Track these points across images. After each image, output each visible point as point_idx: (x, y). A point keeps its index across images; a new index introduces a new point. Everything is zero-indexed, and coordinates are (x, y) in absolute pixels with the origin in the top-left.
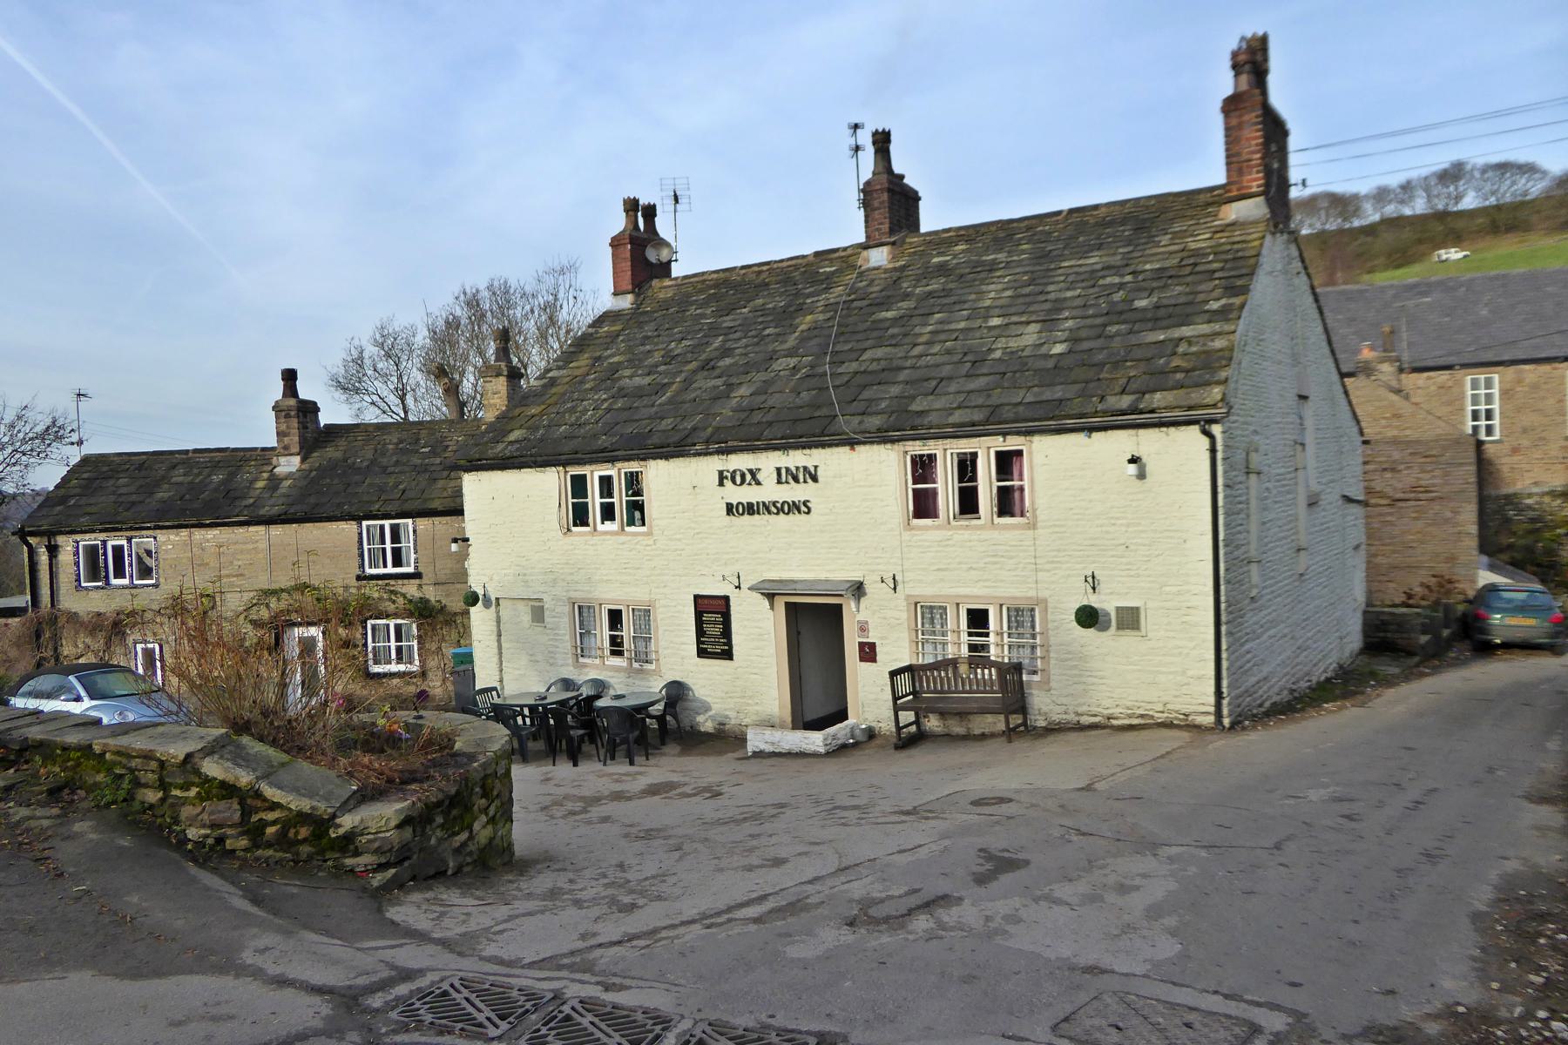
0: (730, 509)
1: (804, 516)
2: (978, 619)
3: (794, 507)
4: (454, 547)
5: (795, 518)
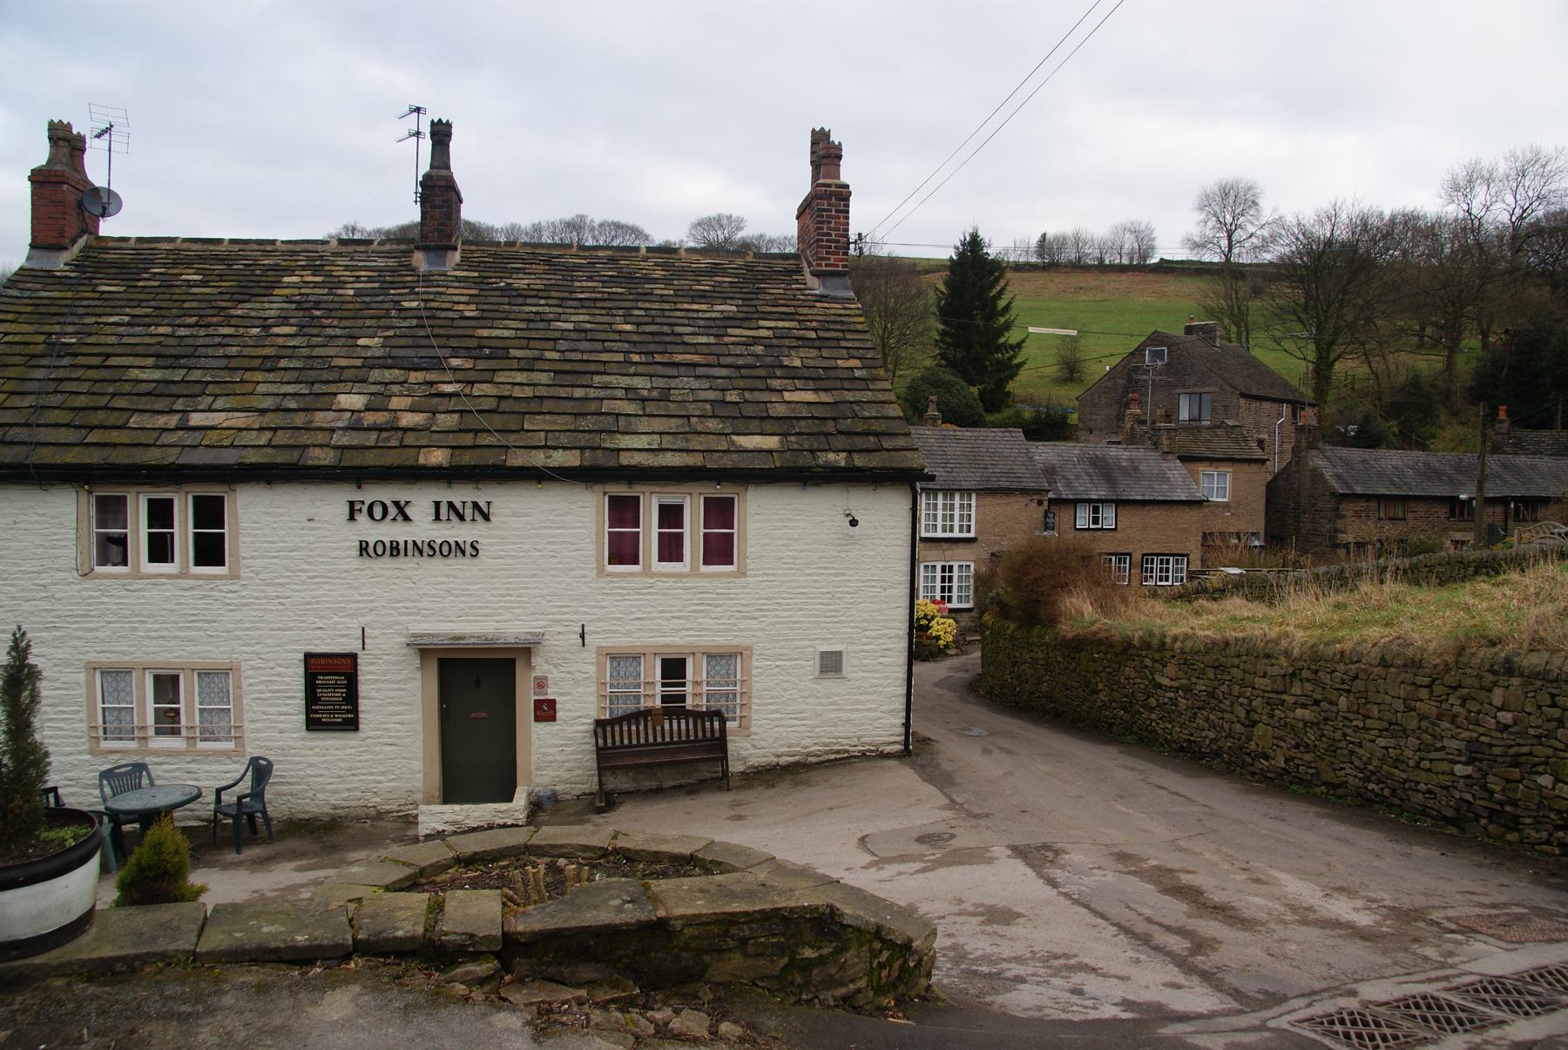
0: (363, 548)
1: (467, 561)
5: (457, 564)
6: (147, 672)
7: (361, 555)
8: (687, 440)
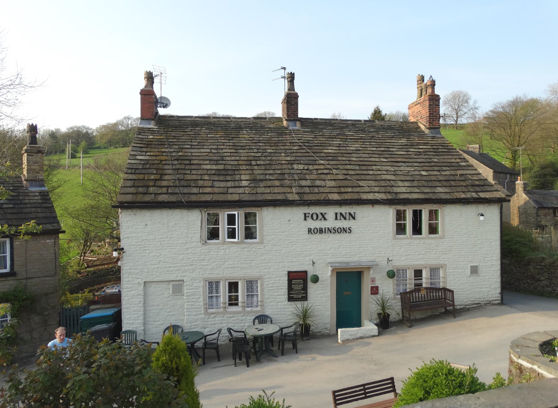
0: (310, 231)
1: (347, 235)
2: (418, 273)
3: (344, 230)
4: (115, 254)
5: (344, 235)
6: (226, 281)
7: (309, 233)
8: (419, 189)
